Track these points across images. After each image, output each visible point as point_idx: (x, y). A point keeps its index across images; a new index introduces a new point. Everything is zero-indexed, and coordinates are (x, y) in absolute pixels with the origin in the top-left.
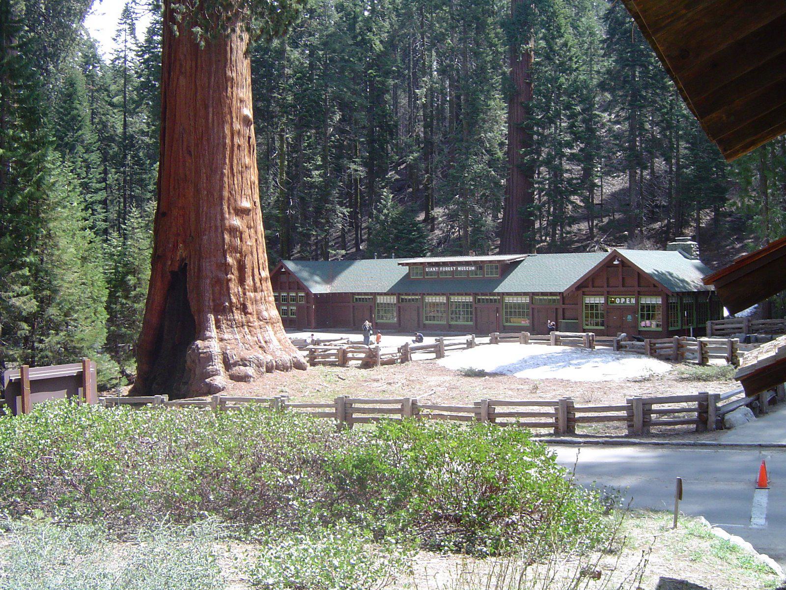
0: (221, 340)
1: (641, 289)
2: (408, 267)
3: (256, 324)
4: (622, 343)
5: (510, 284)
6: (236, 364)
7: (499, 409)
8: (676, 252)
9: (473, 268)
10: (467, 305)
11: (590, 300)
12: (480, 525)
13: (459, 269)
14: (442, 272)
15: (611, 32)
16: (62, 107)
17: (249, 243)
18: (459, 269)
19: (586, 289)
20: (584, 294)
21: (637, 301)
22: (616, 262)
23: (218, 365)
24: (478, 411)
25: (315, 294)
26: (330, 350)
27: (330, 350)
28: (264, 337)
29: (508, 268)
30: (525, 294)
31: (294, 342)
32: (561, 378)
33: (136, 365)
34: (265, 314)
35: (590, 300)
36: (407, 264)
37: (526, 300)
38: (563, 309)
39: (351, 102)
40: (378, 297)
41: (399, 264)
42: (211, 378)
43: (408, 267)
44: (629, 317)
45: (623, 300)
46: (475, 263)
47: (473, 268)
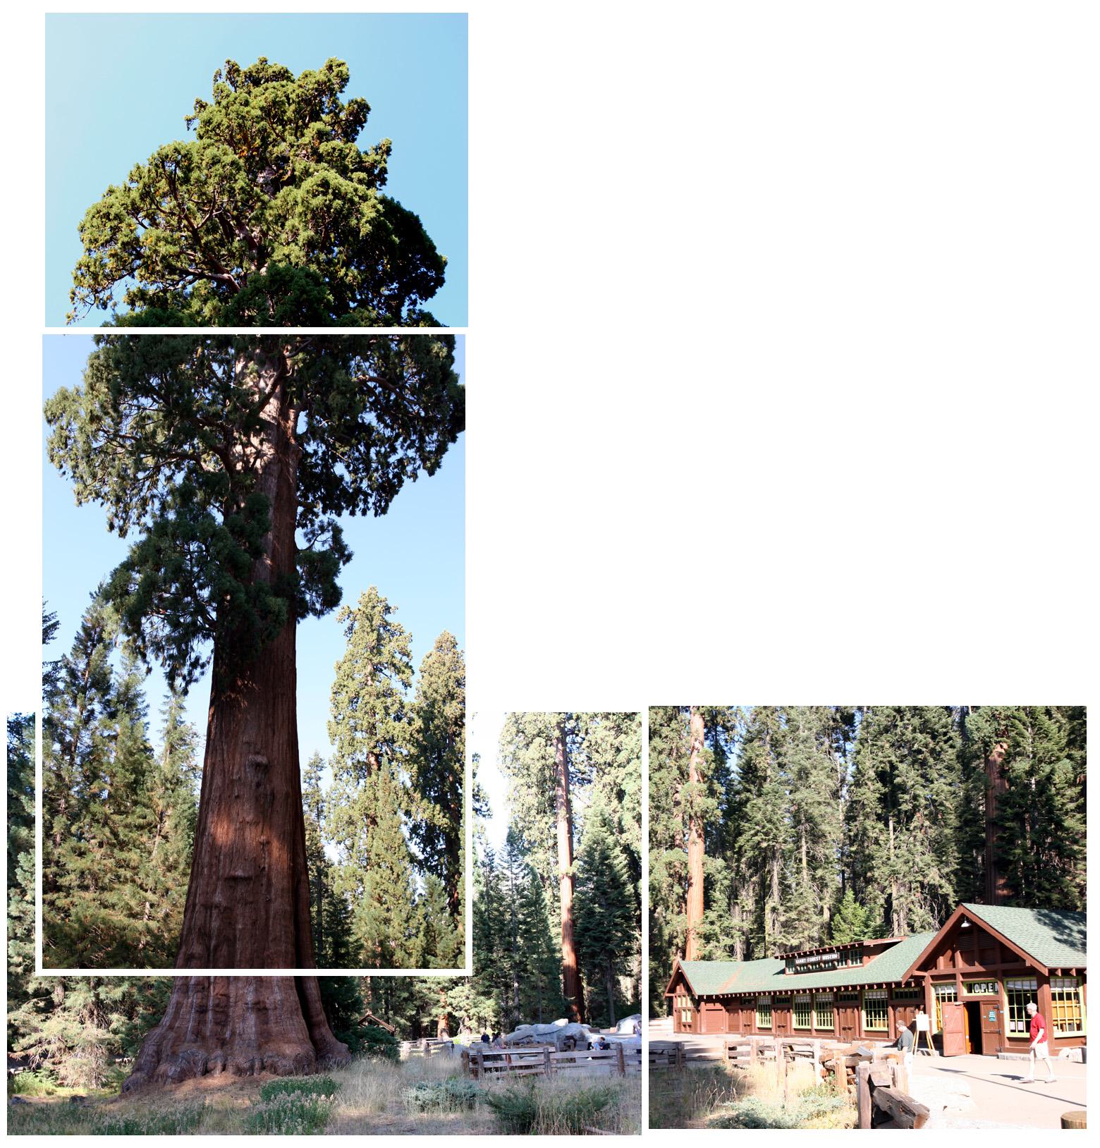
22: (965, 925)
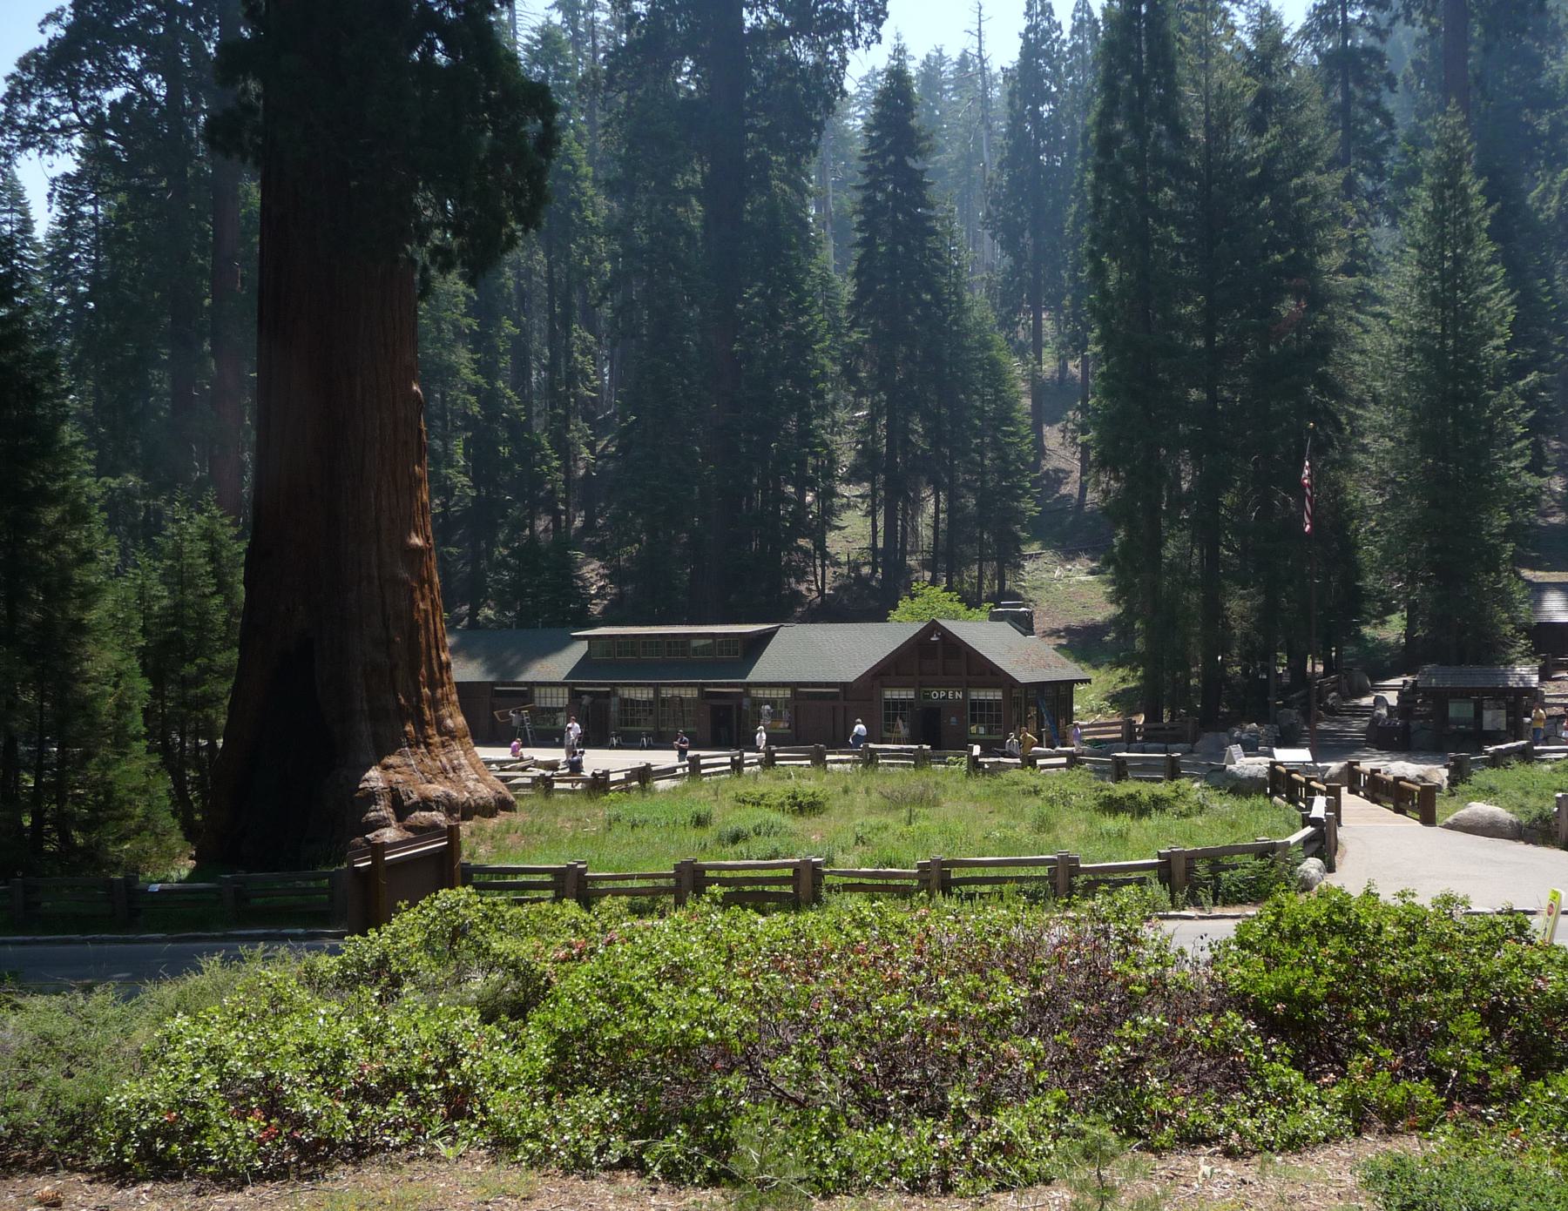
3: (437, 739)
4: (1295, 776)
5: (765, 669)
6: (416, 807)
7: (956, 874)
8: (1005, 624)
11: (891, 694)
12: (1076, 1060)
15: (862, 293)
16: (1013, 434)
17: (422, 606)
21: (966, 695)
23: (384, 810)
24: (924, 877)
26: (516, 777)
27: (516, 777)
28: (451, 761)
29: (758, 643)
31: (1023, 783)
34: (449, 722)
35: (891, 694)
38: (845, 708)
42: (377, 832)
44: (953, 719)
45: (943, 694)
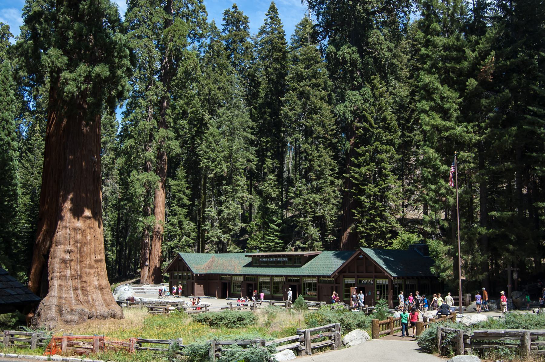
0: (60, 298)
1: (359, 274)
2: (251, 258)
8: (195, 271)
9: (286, 259)
10: (384, 286)
13: (279, 259)
14: (270, 262)
18: (279, 259)
19: (345, 274)
20: (344, 277)
25: (196, 275)
30: (313, 276)
32: (382, 343)
33: (467, 83)
36: (250, 256)
37: (314, 280)
39: (327, 21)
40: (234, 277)
41: (246, 256)
43: (251, 258)
45: (366, 281)
46: (288, 256)
47: (286, 259)
